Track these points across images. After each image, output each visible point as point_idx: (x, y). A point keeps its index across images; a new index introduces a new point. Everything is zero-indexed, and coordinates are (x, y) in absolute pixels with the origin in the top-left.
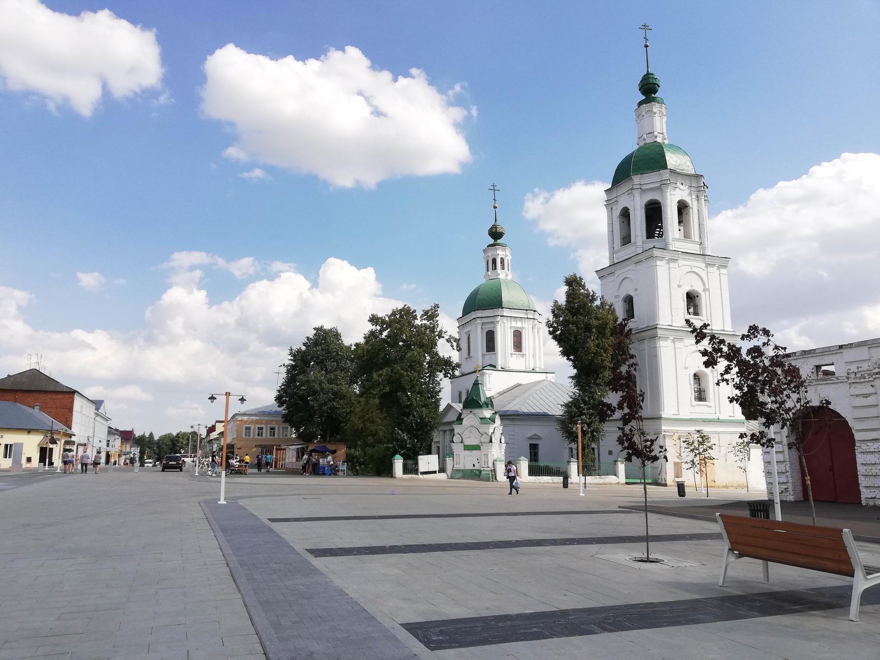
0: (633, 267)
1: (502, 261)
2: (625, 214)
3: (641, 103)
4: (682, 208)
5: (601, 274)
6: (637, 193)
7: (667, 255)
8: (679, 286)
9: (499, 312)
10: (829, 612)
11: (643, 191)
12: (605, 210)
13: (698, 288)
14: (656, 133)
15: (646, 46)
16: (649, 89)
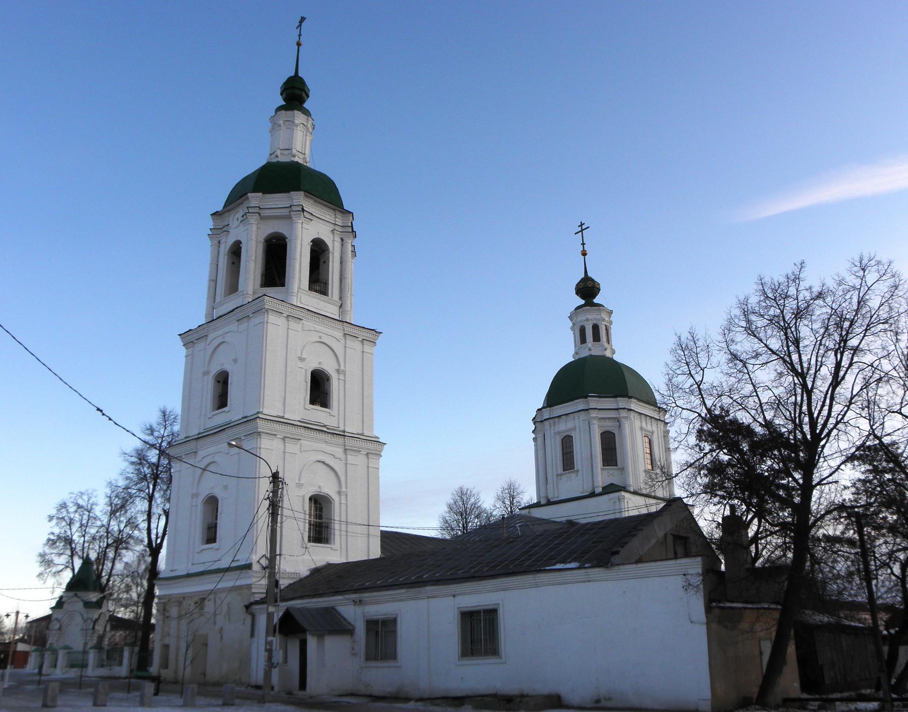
0: (234, 326)
1: (596, 328)
2: (236, 251)
3: (279, 109)
4: (319, 251)
5: (188, 339)
6: (253, 219)
7: (286, 310)
8: (302, 359)
9: (622, 402)
10: (446, 695)
11: (263, 218)
12: (208, 243)
13: (329, 367)
14: (294, 151)
15: (299, 44)
16: (294, 94)
